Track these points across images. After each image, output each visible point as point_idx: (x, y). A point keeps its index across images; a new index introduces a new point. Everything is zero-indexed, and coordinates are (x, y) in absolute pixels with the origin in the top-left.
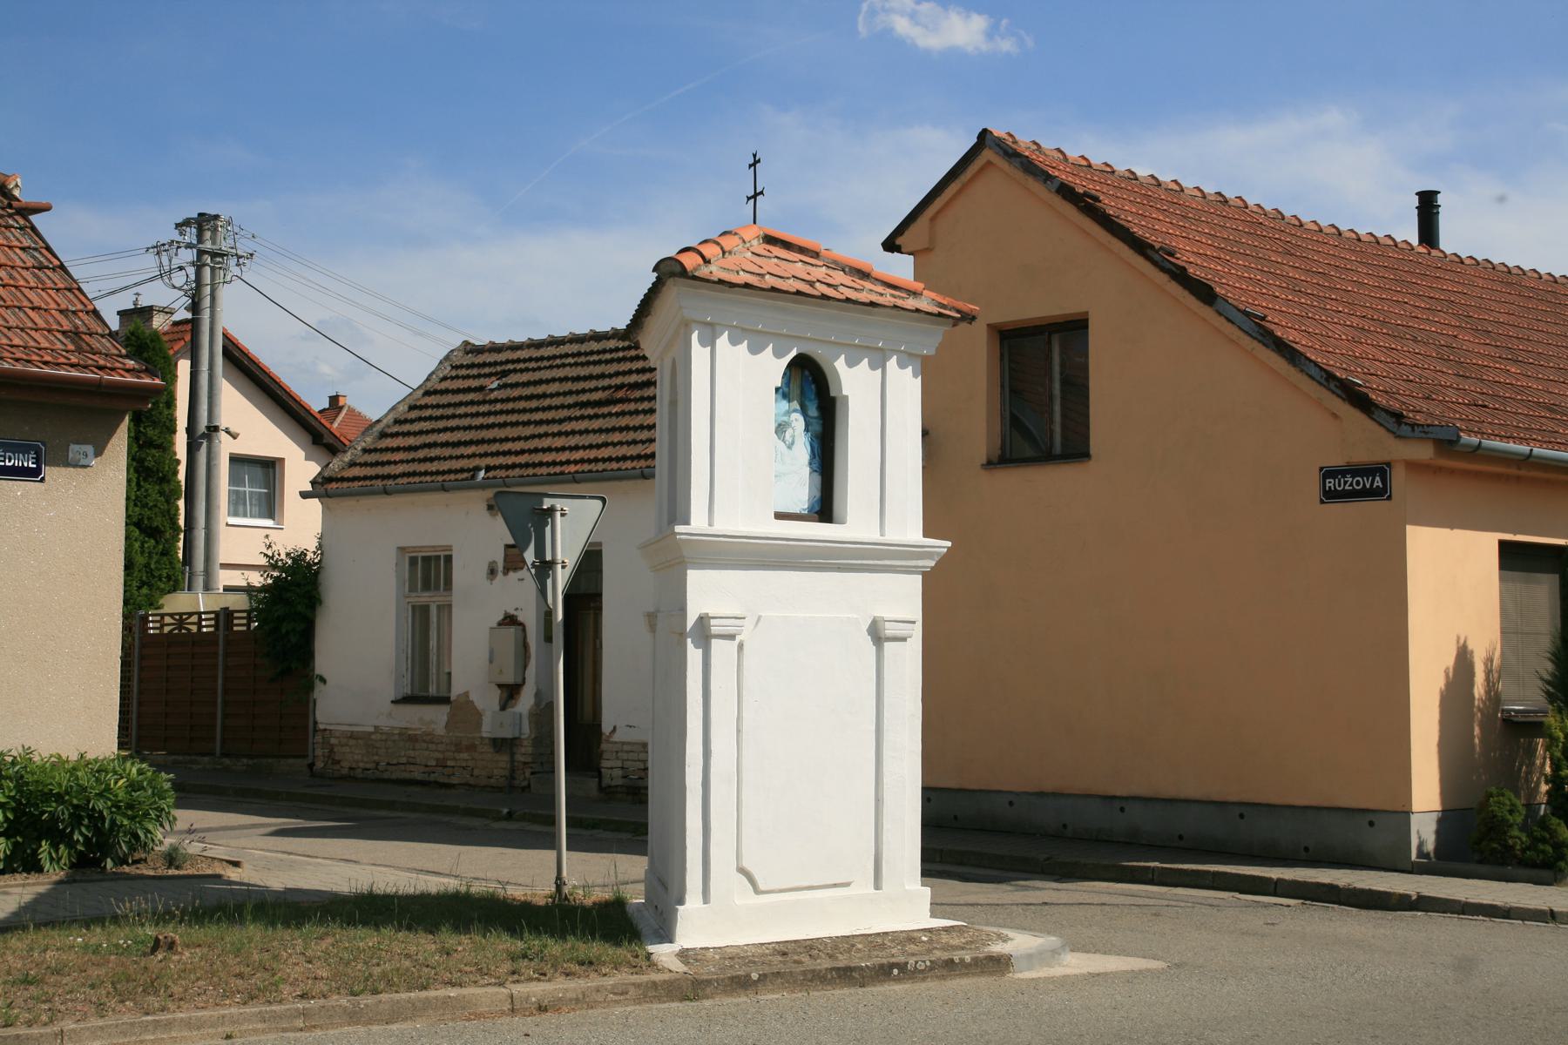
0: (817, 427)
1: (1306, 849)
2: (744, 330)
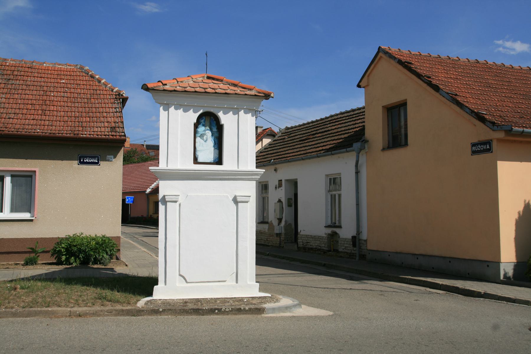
0: (217, 135)
1: (469, 274)
2: (180, 105)
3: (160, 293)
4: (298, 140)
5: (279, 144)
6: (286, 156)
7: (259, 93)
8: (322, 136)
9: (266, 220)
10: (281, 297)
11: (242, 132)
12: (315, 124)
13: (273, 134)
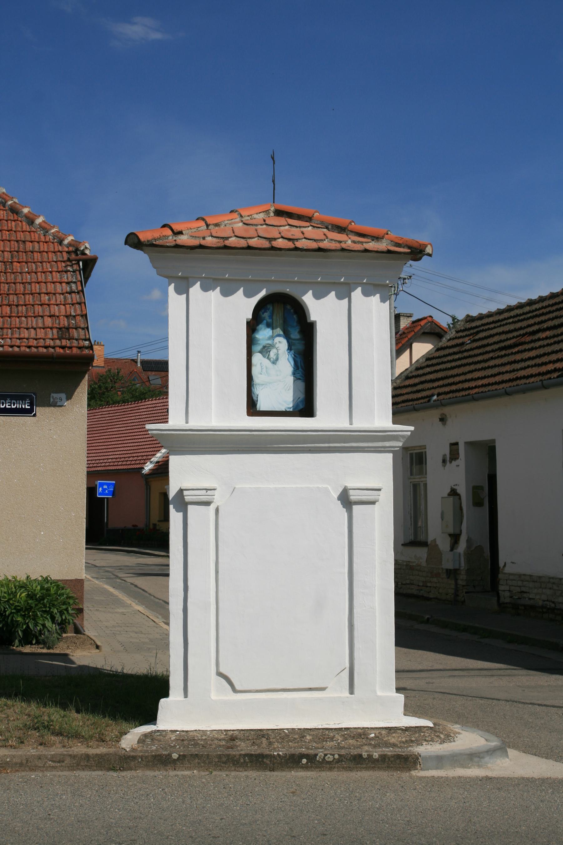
0: (300, 346)
2: (215, 280)
3: (175, 716)
4: (496, 346)
5: (449, 358)
6: (466, 385)
7: (398, 245)
8: (554, 336)
9: (422, 538)
10: (456, 728)
11: (360, 342)
12: (537, 306)
13: (437, 330)
